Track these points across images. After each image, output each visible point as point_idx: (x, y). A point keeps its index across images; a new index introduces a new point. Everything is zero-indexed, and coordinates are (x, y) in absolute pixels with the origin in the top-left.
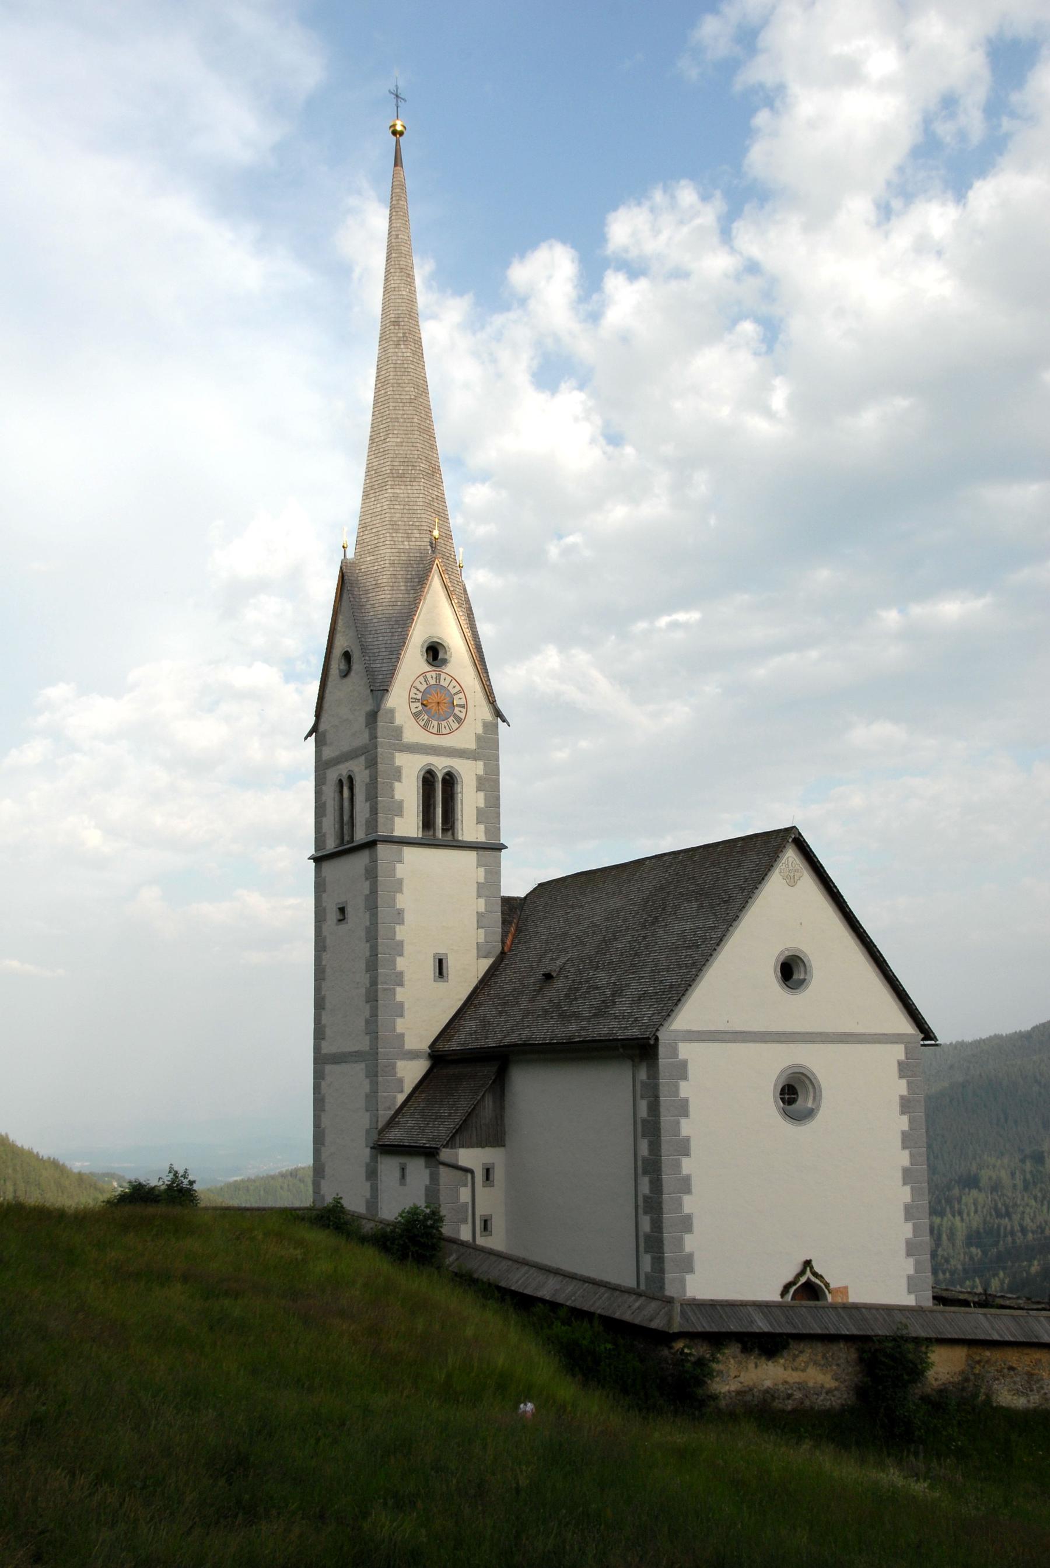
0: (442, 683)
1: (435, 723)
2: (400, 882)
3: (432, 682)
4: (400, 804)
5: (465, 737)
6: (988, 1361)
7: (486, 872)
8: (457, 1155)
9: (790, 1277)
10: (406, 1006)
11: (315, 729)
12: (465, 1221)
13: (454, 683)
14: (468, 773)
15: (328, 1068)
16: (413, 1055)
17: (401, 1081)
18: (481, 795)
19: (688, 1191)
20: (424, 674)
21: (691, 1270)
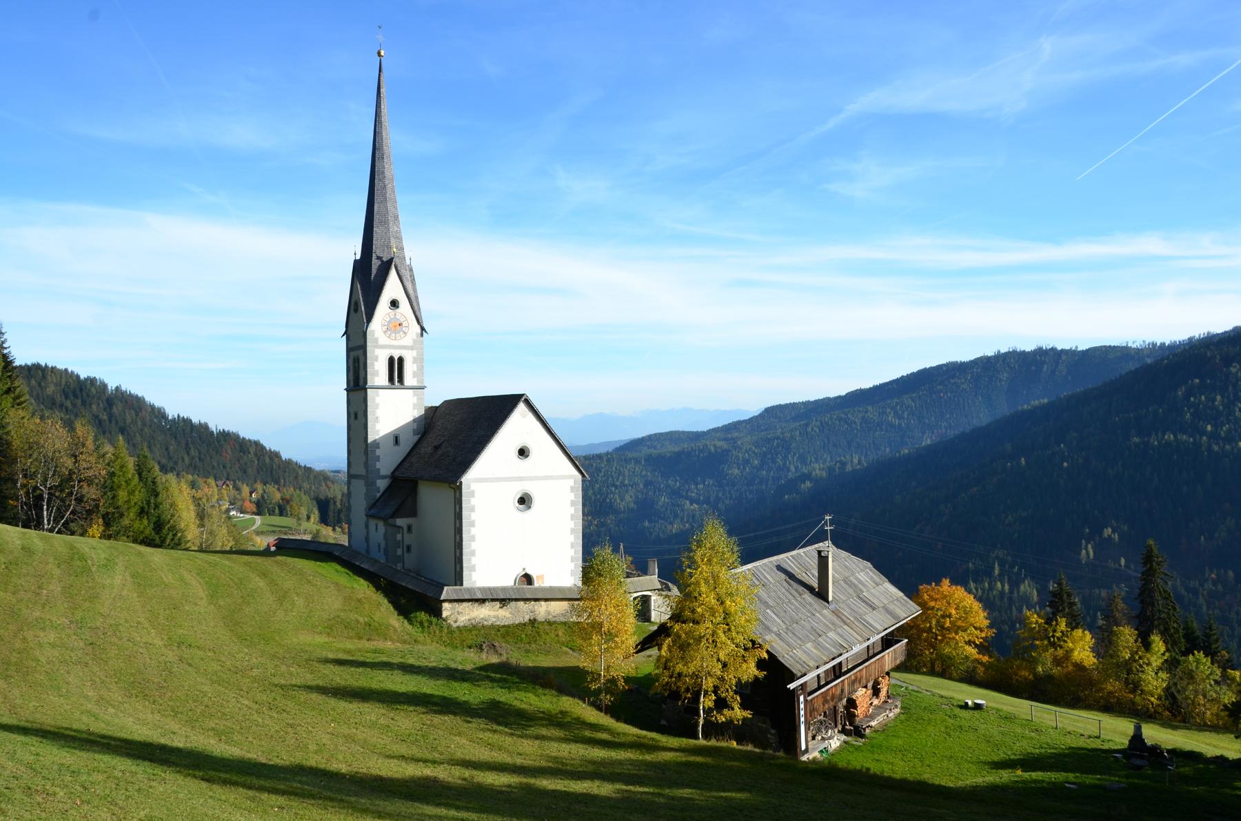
0: (397, 317)
2: (378, 405)
3: (393, 317)
4: (377, 372)
7: (418, 399)
8: (395, 521)
10: (381, 457)
11: (345, 333)
12: (399, 547)
13: (403, 317)
15: (353, 480)
16: (384, 477)
17: (379, 488)
18: (415, 365)
19: (474, 540)
20: (388, 314)
21: (475, 570)
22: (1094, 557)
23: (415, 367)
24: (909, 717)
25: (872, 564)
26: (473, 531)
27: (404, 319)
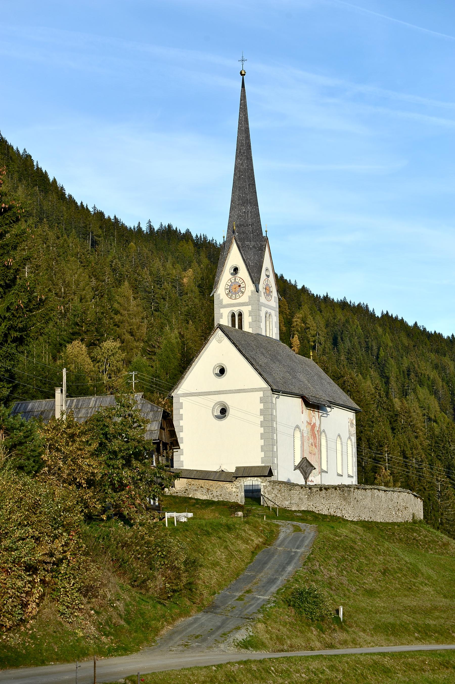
1: (234, 295)
9: (278, 444)
13: (241, 280)
20: (230, 279)
22: (54, 391)
23: (250, 319)
26: (182, 423)
27: (242, 281)
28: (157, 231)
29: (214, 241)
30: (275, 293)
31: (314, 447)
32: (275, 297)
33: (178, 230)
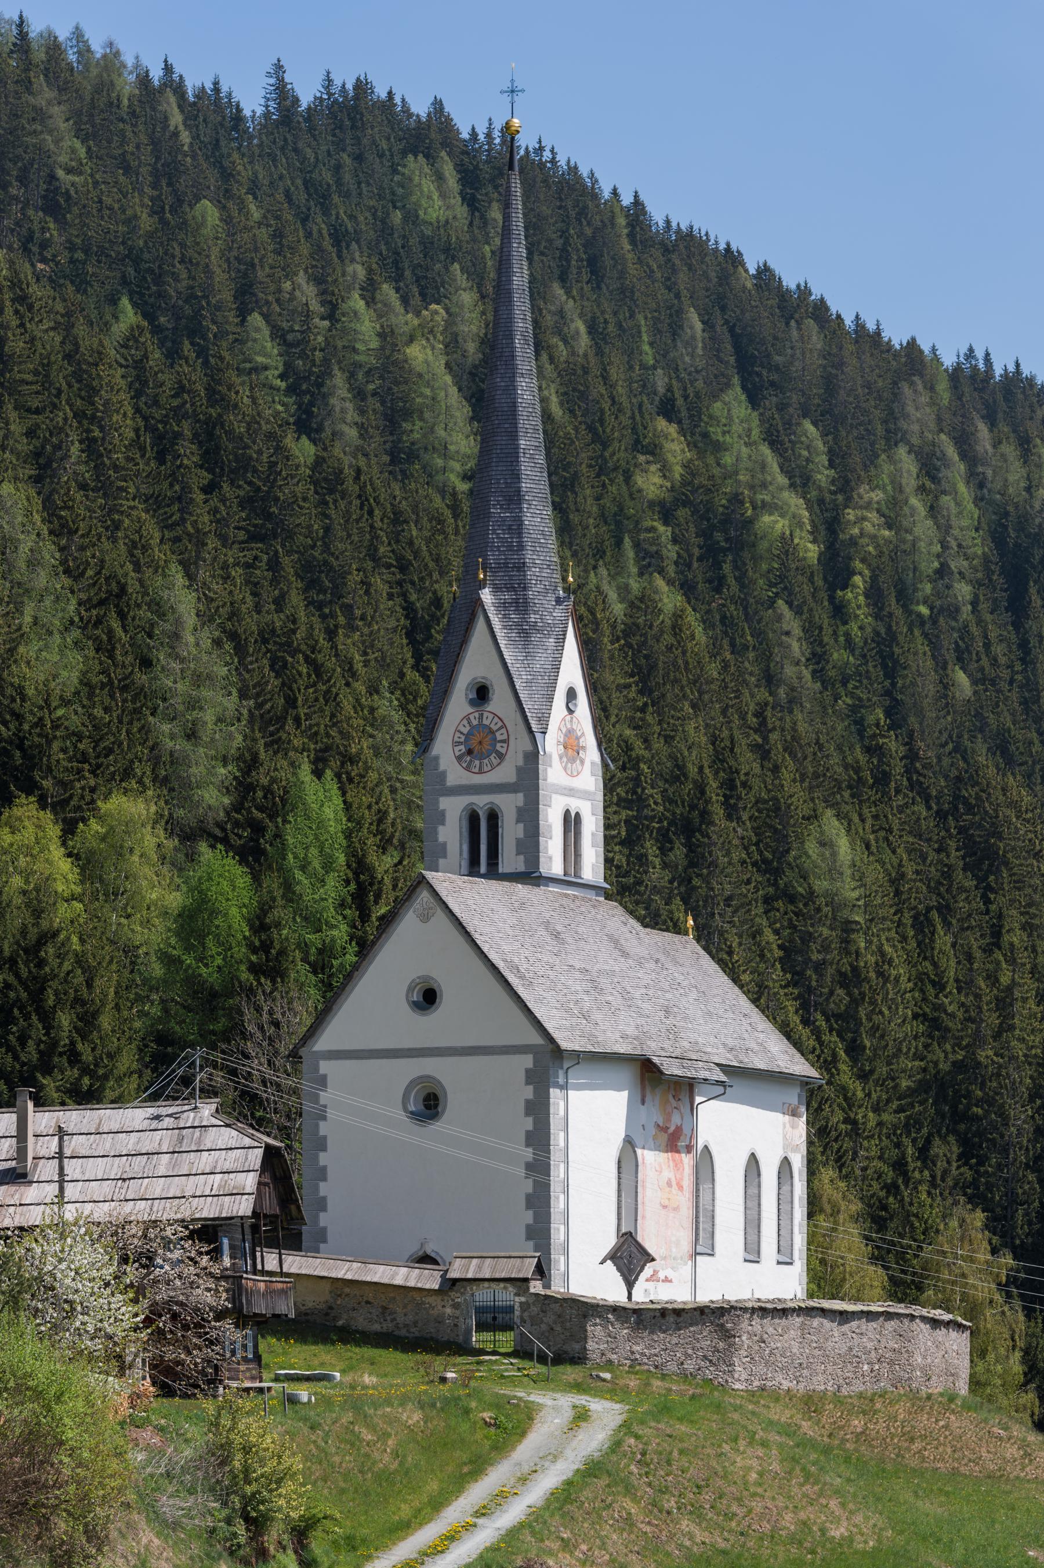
1: (477, 762)
5: (505, 773)
6: (347, 1295)
13: (496, 719)
14: (508, 805)
20: (467, 717)
24: (544, 1551)
25: (517, 477)
27: (500, 724)
28: (309, 108)
29: (547, 155)
30: (592, 754)
31: (675, 1190)
32: (593, 763)
33: (398, 100)
